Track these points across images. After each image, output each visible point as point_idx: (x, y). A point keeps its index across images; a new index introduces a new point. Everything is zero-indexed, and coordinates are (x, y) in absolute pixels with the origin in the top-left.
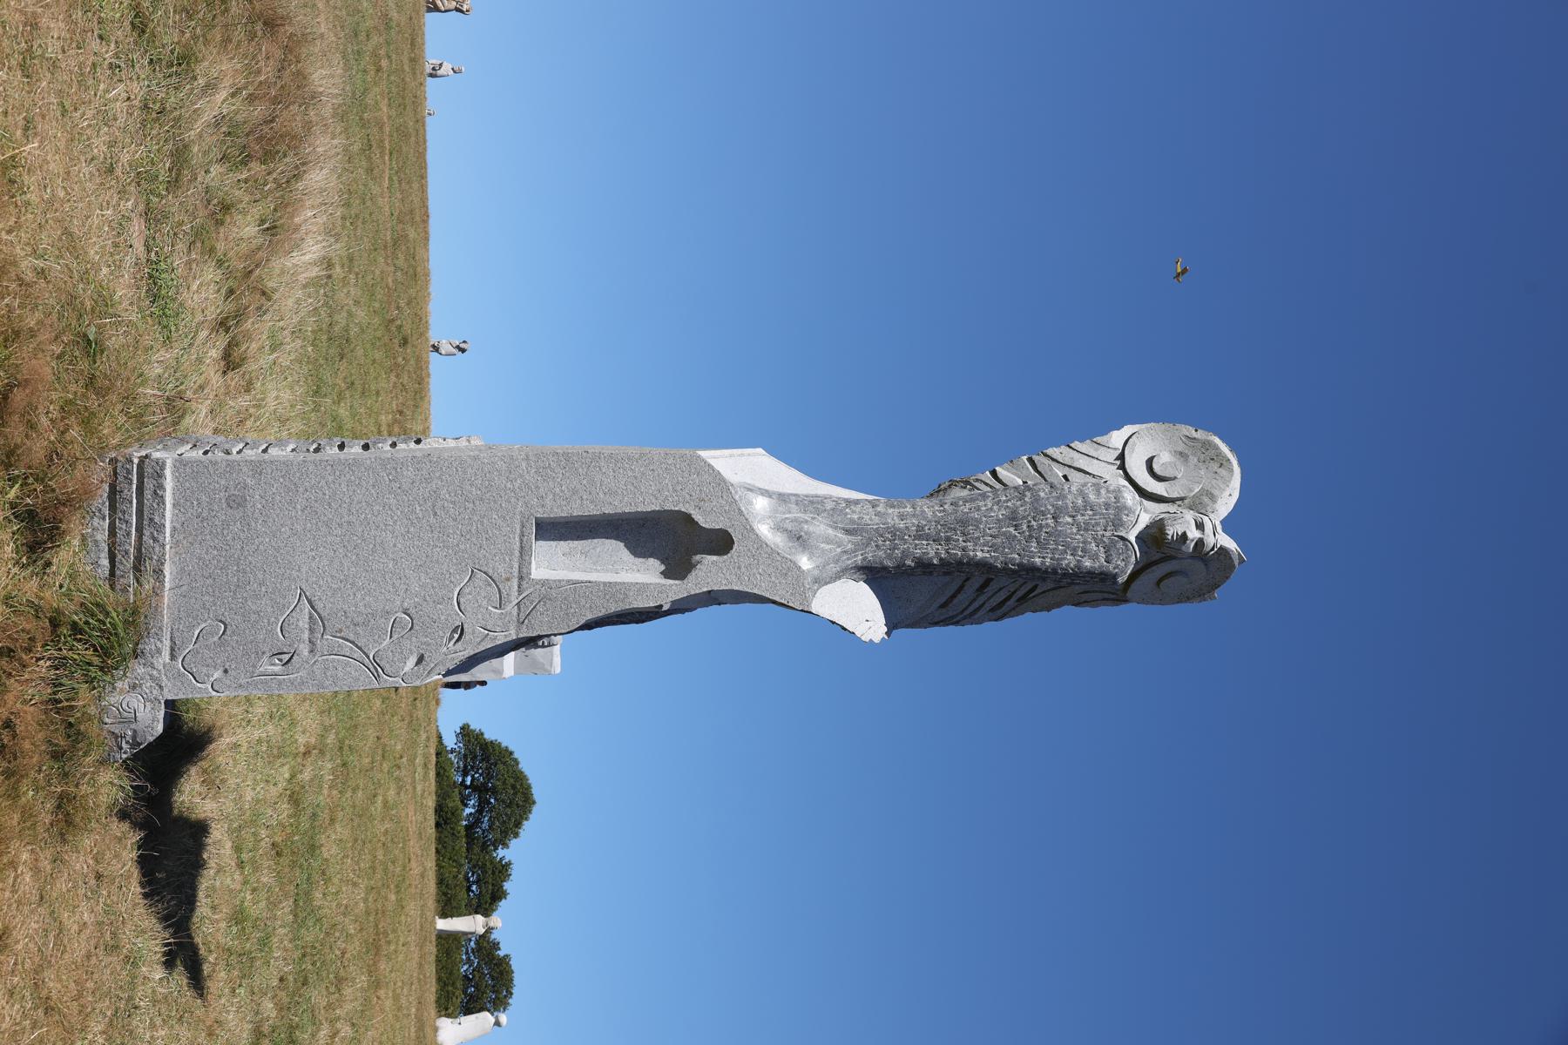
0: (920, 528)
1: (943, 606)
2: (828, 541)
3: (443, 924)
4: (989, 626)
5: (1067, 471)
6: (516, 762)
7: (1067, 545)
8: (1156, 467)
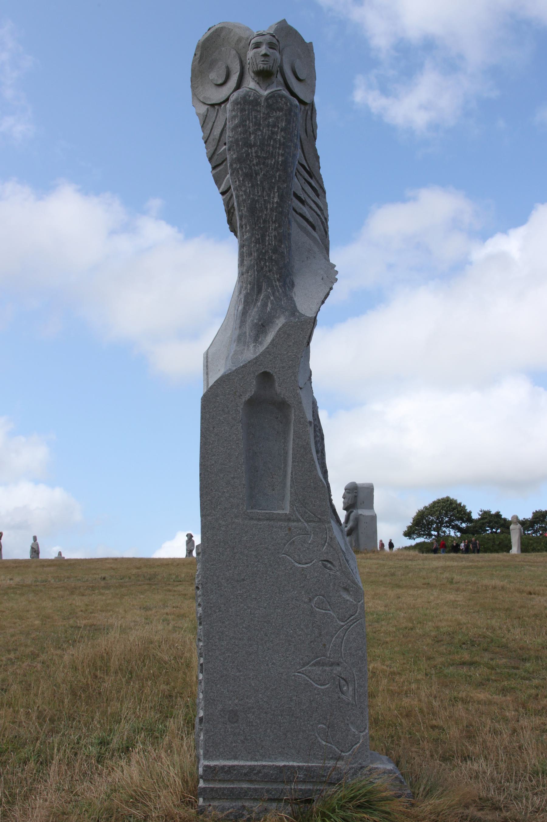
0: (257, 242)
1: (314, 228)
2: (265, 305)
3: (515, 550)
4: (330, 198)
5: (221, 143)
6: (426, 508)
7: (270, 138)
8: (220, 82)
